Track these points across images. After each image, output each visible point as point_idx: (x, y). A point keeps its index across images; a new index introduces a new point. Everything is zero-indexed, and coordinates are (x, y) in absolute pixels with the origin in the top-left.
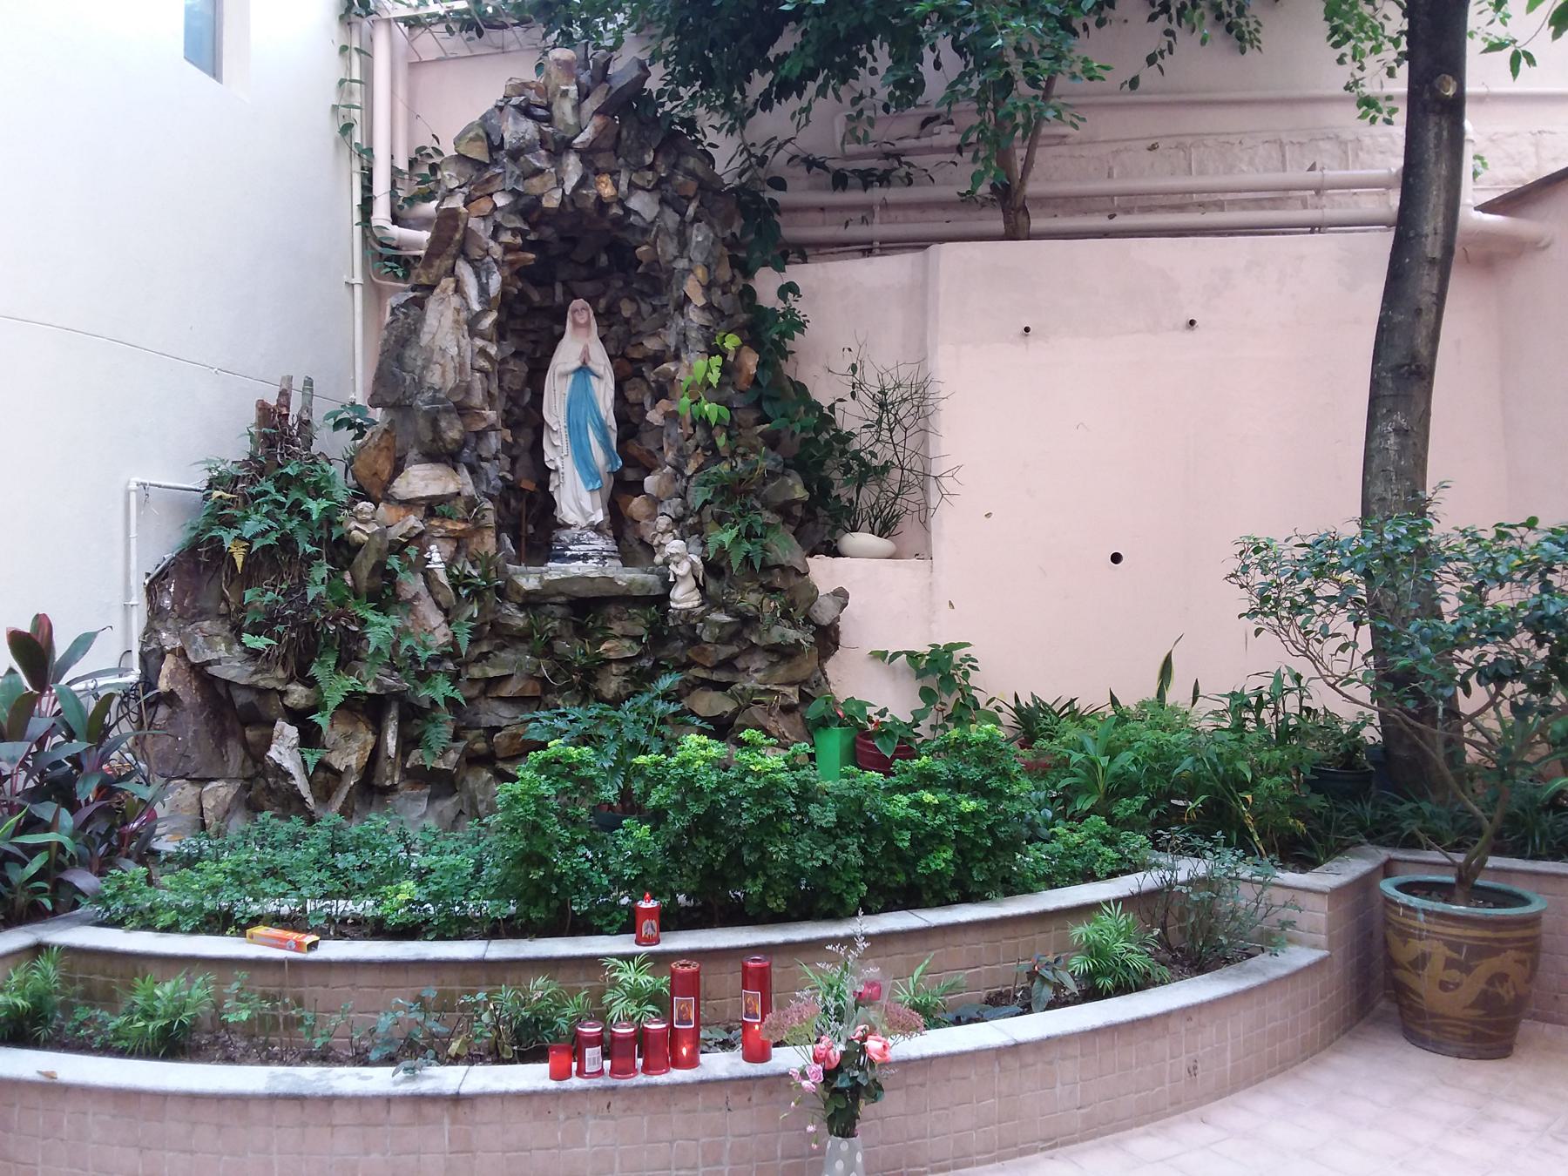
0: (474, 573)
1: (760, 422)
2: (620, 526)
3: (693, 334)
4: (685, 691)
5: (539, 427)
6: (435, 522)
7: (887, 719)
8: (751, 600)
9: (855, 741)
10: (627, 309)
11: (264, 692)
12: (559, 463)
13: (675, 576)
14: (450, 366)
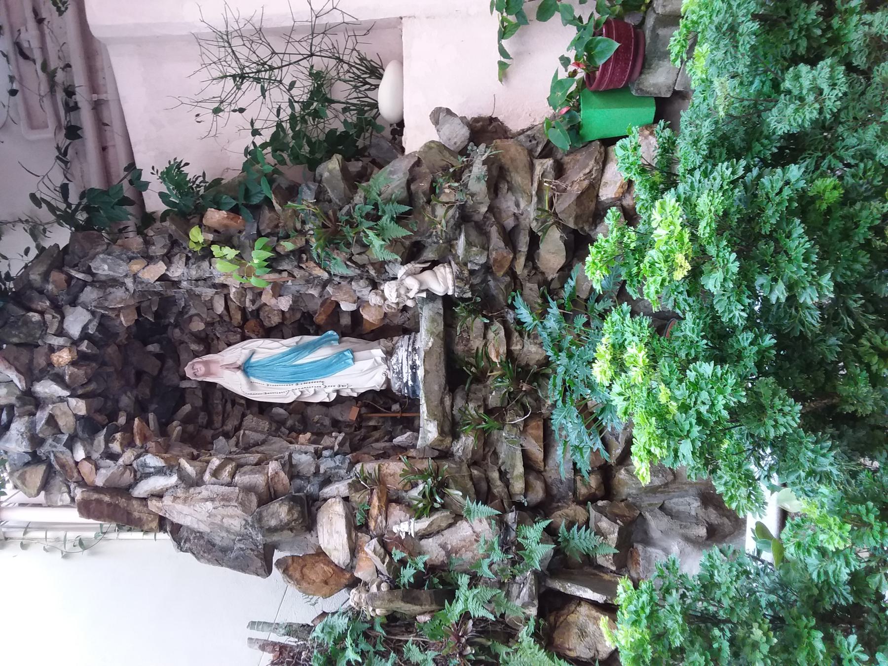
0: (421, 487)
1: (271, 207)
2: (394, 328)
3: (194, 273)
4: (540, 277)
5: (299, 408)
6: (372, 525)
7: (571, 55)
8: (442, 215)
9: (596, 92)
10: (198, 326)
13: (421, 291)
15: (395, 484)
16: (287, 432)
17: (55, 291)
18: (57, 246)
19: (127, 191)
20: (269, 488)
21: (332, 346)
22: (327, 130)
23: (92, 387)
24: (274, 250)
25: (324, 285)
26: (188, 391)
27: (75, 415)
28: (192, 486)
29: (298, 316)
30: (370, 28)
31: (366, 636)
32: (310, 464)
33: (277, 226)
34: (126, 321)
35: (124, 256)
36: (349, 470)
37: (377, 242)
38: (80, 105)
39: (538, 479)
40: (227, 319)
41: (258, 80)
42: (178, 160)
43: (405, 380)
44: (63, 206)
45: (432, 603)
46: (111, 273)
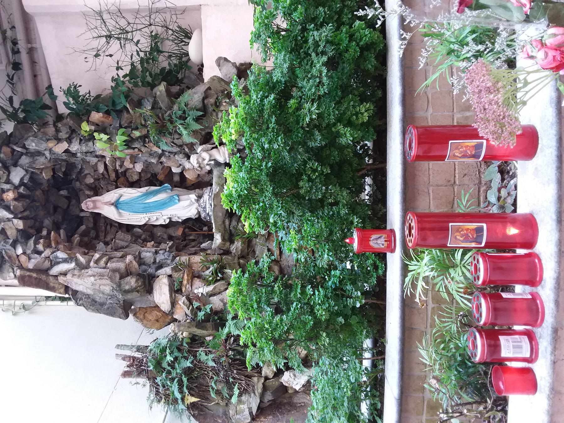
1: (128, 112)
3: (84, 149)
6: (184, 289)
10: (90, 180)
11: (265, 388)
12: (165, 217)
13: (210, 160)
14: (99, 282)
15: (197, 268)
16: (142, 242)
17: (5, 158)
18: (6, 132)
19: (47, 100)
20: (127, 270)
21: (166, 192)
22: (160, 68)
23: (25, 214)
24: (129, 136)
25: (160, 156)
26: (85, 218)
27: (17, 229)
28: (83, 269)
29: (149, 175)
30: (184, 10)
31: (179, 350)
32: (151, 258)
33: (131, 122)
34: (46, 176)
35: (44, 139)
36: (173, 260)
37: (184, 132)
38: (20, 50)
39: (276, 265)
40: (107, 176)
41: (119, 39)
42: (75, 84)
43: (207, 212)
44: (11, 110)
45: (213, 330)
46: (37, 148)
